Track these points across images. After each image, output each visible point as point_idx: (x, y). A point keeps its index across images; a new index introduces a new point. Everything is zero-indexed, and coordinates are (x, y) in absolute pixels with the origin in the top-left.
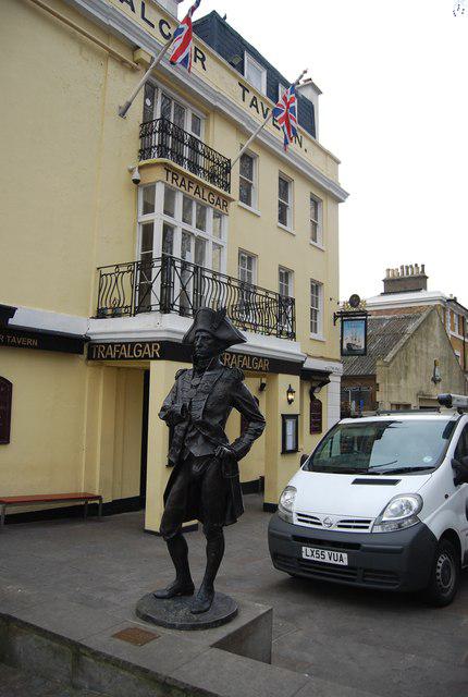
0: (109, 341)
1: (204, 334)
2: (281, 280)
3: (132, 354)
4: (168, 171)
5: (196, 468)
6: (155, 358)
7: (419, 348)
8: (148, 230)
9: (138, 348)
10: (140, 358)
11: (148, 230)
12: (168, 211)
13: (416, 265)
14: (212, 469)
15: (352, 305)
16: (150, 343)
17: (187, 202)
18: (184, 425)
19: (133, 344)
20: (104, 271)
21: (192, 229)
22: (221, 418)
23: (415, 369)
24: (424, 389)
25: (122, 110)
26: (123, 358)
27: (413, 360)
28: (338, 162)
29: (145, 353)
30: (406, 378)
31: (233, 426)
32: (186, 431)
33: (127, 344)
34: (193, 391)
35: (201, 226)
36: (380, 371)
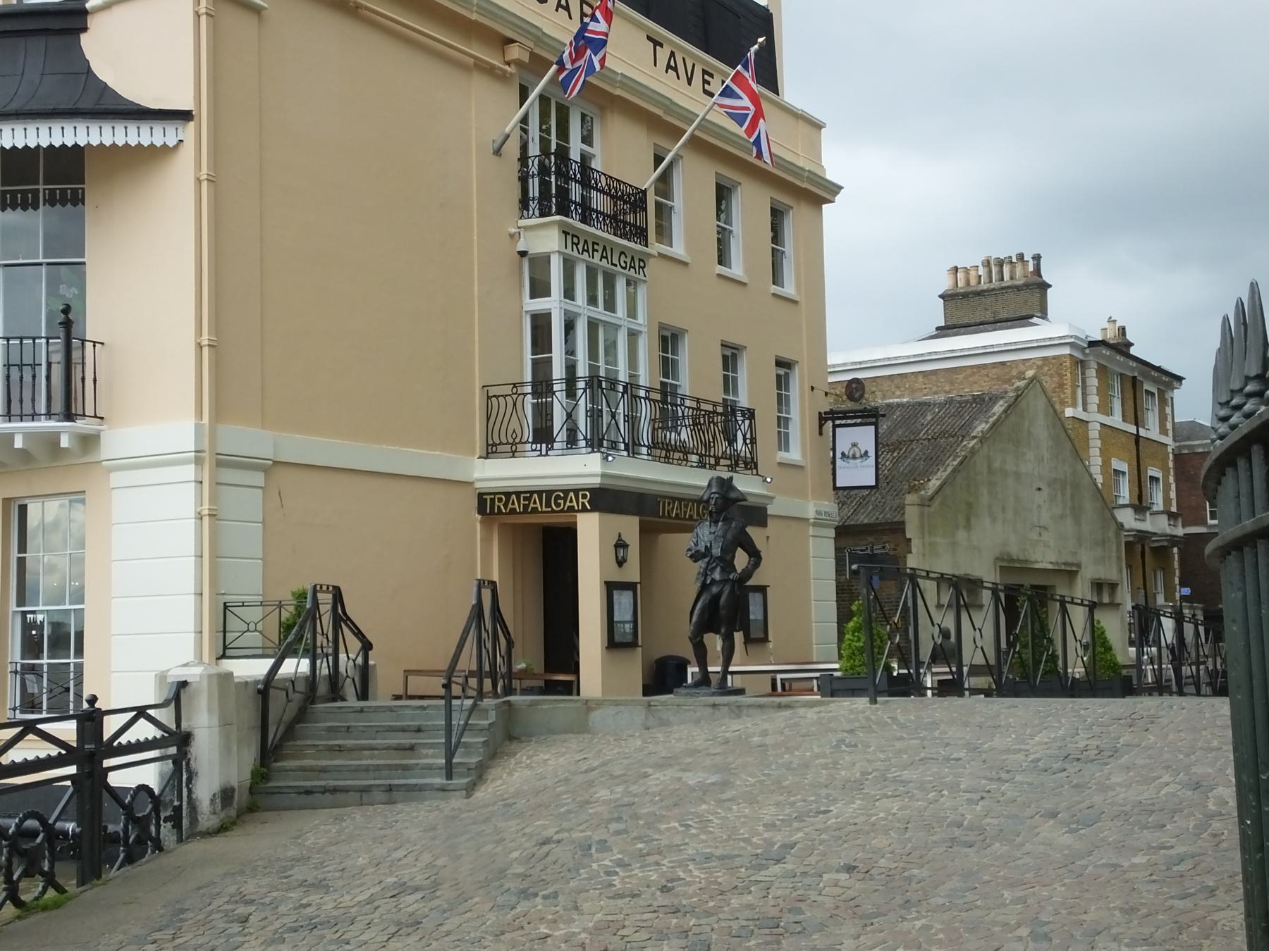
0: (511, 490)
1: (717, 495)
2: (725, 368)
3: (548, 505)
4: (566, 233)
5: (715, 590)
6: (584, 510)
7: (997, 465)
8: (541, 324)
9: (558, 497)
10: (562, 511)
11: (541, 324)
12: (569, 293)
13: (1021, 257)
14: (727, 590)
15: (851, 397)
16: (576, 491)
17: (591, 273)
18: (706, 560)
19: (550, 493)
20: (493, 391)
21: (599, 312)
22: (731, 555)
23: (990, 507)
24: (1014, 551)
25: (496, 146)
26: (535, 510)
27: (984, 491)
28: (818, 126)
29: (568, 504)
30: (968, 527)
31: (741, 560)
32: (708, 563)
33: (540, 493)
34: (713, 536)
35: (610, 306)
36: (912, 517)
